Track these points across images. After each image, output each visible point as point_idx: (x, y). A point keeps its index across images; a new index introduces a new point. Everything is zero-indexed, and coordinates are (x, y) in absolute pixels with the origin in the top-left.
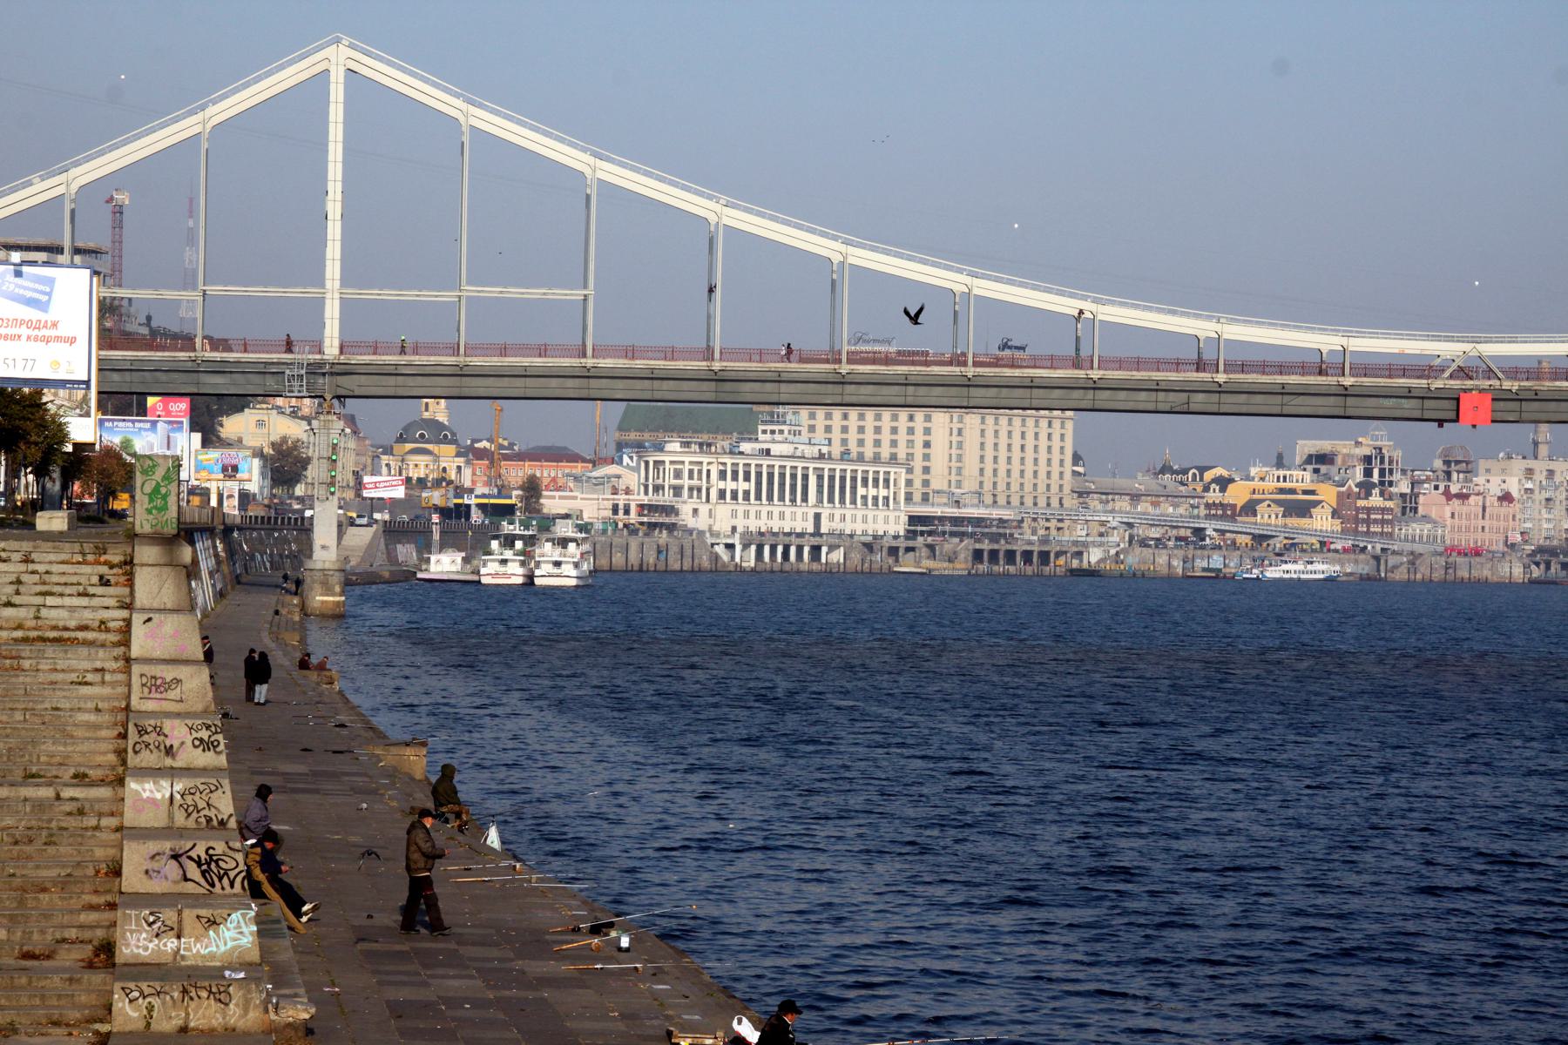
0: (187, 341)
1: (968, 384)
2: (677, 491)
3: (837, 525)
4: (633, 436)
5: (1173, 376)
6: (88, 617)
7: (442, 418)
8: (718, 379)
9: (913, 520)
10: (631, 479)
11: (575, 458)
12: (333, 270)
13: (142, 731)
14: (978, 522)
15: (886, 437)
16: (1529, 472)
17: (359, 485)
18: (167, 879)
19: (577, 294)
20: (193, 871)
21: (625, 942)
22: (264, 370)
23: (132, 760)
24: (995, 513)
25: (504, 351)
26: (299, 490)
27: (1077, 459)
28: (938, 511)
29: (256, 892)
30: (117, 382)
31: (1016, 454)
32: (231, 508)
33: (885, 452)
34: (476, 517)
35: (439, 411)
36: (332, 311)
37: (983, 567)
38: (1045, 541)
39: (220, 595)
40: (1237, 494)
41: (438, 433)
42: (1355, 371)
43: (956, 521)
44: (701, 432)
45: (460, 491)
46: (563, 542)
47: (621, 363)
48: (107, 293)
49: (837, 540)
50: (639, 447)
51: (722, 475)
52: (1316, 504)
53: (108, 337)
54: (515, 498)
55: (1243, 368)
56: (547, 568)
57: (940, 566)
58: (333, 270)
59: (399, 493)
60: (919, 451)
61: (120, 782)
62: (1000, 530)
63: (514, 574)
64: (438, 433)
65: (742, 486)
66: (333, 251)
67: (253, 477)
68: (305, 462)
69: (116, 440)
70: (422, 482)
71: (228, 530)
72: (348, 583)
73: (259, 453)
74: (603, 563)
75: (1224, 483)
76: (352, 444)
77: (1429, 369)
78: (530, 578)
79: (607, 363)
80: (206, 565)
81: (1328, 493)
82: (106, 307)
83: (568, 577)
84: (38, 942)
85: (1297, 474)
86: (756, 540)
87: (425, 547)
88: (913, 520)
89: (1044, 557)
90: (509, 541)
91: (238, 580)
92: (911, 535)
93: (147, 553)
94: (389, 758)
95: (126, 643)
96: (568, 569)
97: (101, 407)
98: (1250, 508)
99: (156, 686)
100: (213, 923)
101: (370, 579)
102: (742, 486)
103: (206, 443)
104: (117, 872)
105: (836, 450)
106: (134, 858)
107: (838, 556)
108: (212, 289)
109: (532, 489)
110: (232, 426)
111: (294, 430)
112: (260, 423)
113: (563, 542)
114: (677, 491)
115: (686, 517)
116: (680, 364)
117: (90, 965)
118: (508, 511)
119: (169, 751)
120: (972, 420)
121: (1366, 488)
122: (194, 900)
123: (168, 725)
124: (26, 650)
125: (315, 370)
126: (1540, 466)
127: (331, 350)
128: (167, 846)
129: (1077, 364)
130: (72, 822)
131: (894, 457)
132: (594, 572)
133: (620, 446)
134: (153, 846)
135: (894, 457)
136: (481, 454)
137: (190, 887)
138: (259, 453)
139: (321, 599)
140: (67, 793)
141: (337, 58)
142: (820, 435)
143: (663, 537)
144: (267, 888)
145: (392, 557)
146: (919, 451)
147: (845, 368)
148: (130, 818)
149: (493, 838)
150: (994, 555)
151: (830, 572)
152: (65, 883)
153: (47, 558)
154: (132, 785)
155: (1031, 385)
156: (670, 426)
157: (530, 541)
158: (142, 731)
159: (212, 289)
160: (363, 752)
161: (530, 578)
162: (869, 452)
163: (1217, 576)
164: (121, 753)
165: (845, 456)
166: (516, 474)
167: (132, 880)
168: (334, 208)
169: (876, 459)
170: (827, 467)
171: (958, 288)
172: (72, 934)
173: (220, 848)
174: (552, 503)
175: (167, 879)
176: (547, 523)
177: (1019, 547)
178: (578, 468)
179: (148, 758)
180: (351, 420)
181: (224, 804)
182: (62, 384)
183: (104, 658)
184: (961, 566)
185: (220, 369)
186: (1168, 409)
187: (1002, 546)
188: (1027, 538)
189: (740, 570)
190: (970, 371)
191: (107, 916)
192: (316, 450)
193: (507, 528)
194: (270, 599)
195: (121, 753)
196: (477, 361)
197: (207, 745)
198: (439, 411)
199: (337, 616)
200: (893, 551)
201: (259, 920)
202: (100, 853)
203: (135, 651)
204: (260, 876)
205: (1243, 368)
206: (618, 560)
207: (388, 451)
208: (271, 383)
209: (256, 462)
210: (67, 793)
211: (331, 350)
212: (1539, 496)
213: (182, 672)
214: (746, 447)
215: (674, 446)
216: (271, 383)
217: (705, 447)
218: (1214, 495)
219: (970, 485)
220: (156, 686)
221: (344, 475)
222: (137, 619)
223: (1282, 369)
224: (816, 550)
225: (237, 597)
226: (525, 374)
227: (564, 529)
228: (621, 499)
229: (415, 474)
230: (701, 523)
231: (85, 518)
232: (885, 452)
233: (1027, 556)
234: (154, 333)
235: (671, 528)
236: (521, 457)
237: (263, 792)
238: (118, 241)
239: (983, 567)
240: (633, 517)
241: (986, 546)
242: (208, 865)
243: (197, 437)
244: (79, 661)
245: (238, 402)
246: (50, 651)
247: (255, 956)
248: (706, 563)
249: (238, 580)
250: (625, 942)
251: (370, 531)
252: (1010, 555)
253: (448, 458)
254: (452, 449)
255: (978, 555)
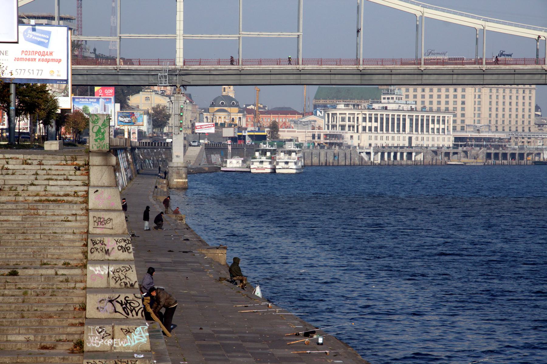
0: (113, 60)
1: (483, 73)
2: (343, 127)
3: (420, 143)
4: (322, 102)
6: (69, 190)
7: (232, 95)
8: (362, 73)
9: (457, 139)
10: (321, 122)
11: (294, 113)
12: (180, 26)
13: (94, 243)
14: (489, 139)
15: (443, 100)
17: (193, 126)
18: (107, 312)
19: (295, 35)
20: (119, 308)
21: (321, 340)
22: (149, 73)
23: (90, 256)
24: (497, 135)
25: (260, 62)
26: (166, 130)
27: (537, 108)
28: (469, 135)
29: (148, 317)
30: (81, 80)
32: (134, 138)
33: (443, 107)
34: (248, 141)
35: (230, 91)
37: (491, 162)
38: (522, 148)
39: (130, 179)
41: (230, 102)
43: (478, 139)
45: (240, 129)
46: (289, 153)
47: (316, 67)
48: (75, 38)
49: (421, 149)
50: (325, 107)
53: (76, 59)
54: (266, 132)
56: (282, 165)
57: (470, 161)
58: (180, 26)
59: (212, 130)
61: (85, 266)
62: (500, 143)
63: (267, 168)
64: (230, 102)
65: (374, 124)
66: (180, 17)
67: (145, 125)
68: (168, 117)
69: (80, 107)
70: (223, 125)
71: (133, 149)
72: (189, 173)
73: (147, 113)
74: (308, 162)
76: (190, 108)
78: (274, 169)
79: (309, 67)
80: (123, 165)
82: (75, 46)
83: (292, 169)
84: (48, 342)
86: (381, 150)
87: (224, 156)
88: (457, 139)
89: (521, 156)
90: (264, 152)
91: (138, 172)
92: (456, 146)
93: (95, 160)
94: (209, 254)
95: (86, 202)
96: (292, 165)
97: (73, 92)
99: (101, 222)
100: (128, 332)
101: (199, 171)
102: (374, 124)
103: (122, 108)
104: (84, 309)
105: (419, 106)
106: (92, 302)
107: (420, 157)
108: (124, 36)
109: (274, 127)
110: (134, 100)
111: (163, 101)
113: (289, 153)
114: (343, 127)
115: (347, 140)
117: (72, 352)
118: (263, 138)
119: (107, 252)
120: (485, 90)
122: (119, 321)
123: (106, 240)
124: (40, 206)
125: (172, 73)
127: (179, 63)
128: (107, 296)
129: (537, 62)
130: (63, 285)
132: (304, 166)
133: (315, 107)
134: (100, 296)
136: (250, 112)
137: (117, 315)
138: (147, 113)
139: (177, 180)
140: (61, 272)
142: (411, 100)
144: (153, 316)
145: (209, 161)
146: (459, 106)
147: (423, 67)
148: (89, 284)
149: (258, 292)
150: (496, 155)
151: (416, 164)
152: (61, 314)
153: (49, 163)
154: (90, 268)
155: (515, 73)
156: (339, 97)
157: (274, 152)
158: (94, 243)
159: (124, 36)
160: (197, 252)
161: (274, 169)
162: (435, 107)
163: (465, 165)
164: (85, 253)
165: (423, 109)
166: (267, 120)
167: (91, 312)
169: (439, 110)
172: (64, 337)
173: (131, 297)
174: (284, 134)
175: (107, 312)
176: (282, 144)
177: (509, 151)
178: (296, 117)
179: (98, 256)
180: (189, 97)
181: (133, 277)
182: (55, 81)
183: (77, 209)
184: (481, 161)
185: (128, 73)
187: (501, 151)
188: (513, 147)
189: (373, 164)
190: (484, 67)
191: (79, 329)
192: (173, 110)
193: (263, 146)
194: (153, 181)
195: (85, 253)
196: (247, 67)
197: (124, 249)
198: (230, 91)
199: (184, 189)
200: (447, 154)
201: (150, 331)
202: (76, 300)
203: (91, 206)
204: (150, 310)
206: (315, 160)
207: (207, 111)
208: (152, 80)
209: (145, 117)
210: (61, 272)
211: (179, 63)
213: (113, 215)
214: (375, 106)
216: (152, 80)
217: (356, 106)
219: (484, 122)
220: (101, 222)
221: (186, 123)
222: (92, 191)
224: (410, 154)
225: (138, 180)
226: (270, 73)
227: (290, 146)
228: (316, 132)
229: (219, 122)
230: (355, 142)
231: (66, 144)
232: (443, 107)
233: (513, 155)
234: (97, 57)
235: (340, 145)
236: (269, 112)
237: (151, 271)
238: (80, 14)
239: (491, 162)
240: (322, 140)
241: (493, 151)
242: (126, 305)
243: (118, 106)
244: (65, 210)
245: (137, 89)
246: (52, 206)
247: (148, 347)
248: (357, 162)
249: (138, 172)
250: (321, 340)
251: (198, 149)
252: (505, 156)
253: (235, 114)
255: (489, 156)
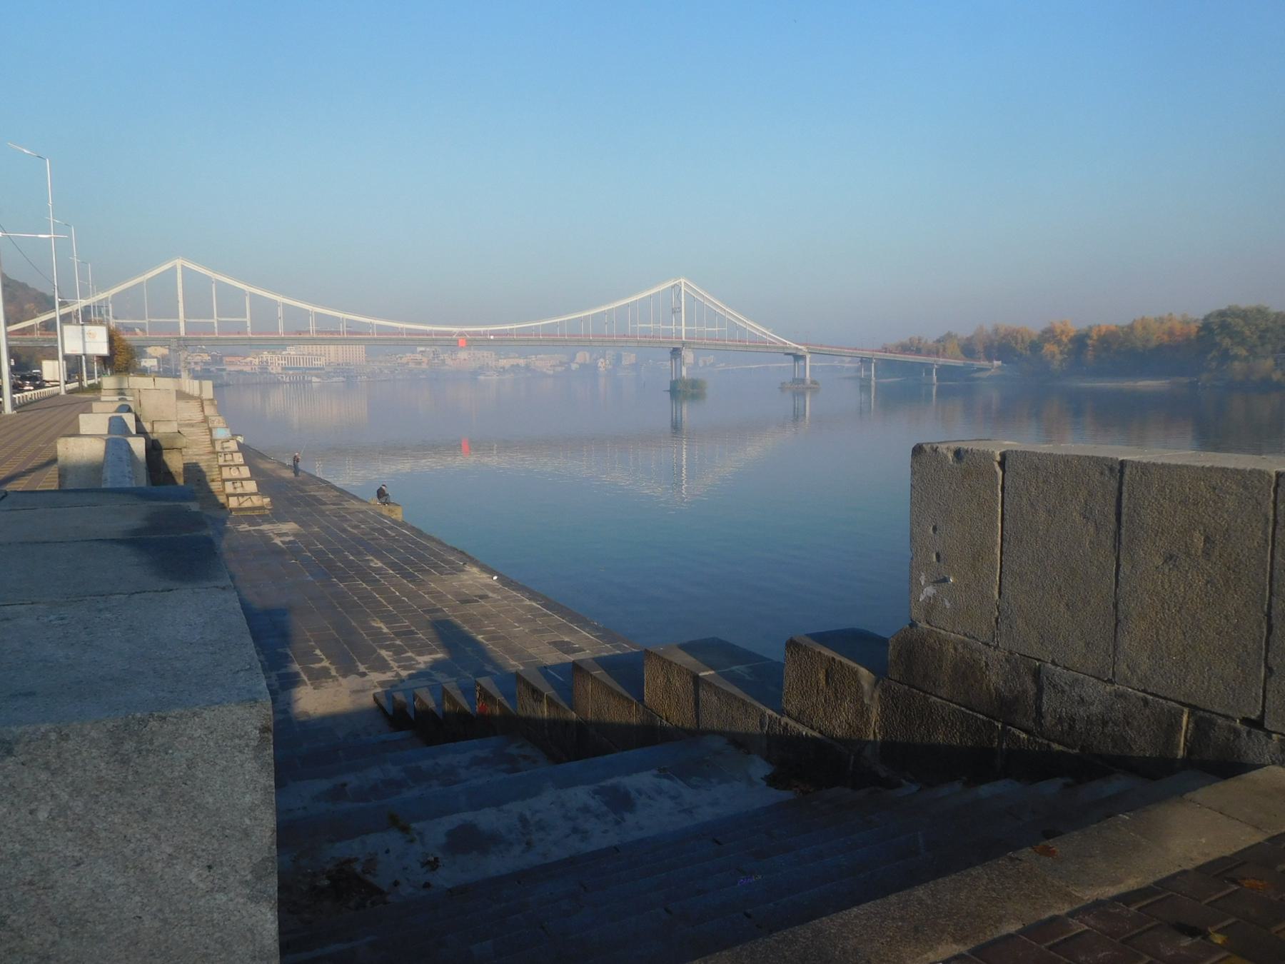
5: (394, 337)
12: (181, 314)
16: (470, 354)
25: (260, 334)
31: (351, 352)
36: (182, 325)
40: (404, 360)
42: (436, 335)
44: (995, 472)
51: (279, 360)
52: (423, 362)
55: (410, 334)
58: (181, 314)
60: (327, 353)
75: (401, 358)
77: (450, 334)
81: (425, 360)
85: (417, 355)
98: (408, 363)
112: (156, 350)
116: (263, 336)
121: (434, 358)
126: (472, 352)
127: (182, 333)
131: (321, 354)
135: (321, 354)
141: (179, 262)
143: (265, 375)
168: (180, 299)
169: (317, 355)
170: (305, 357)
171: (341, 317)
186: (1004, 550)
205: (410, 334)
212: (472, 359)
214: (284, 353)
215: (266, 353)
217: (274, 353)
218: (399, 361)
223: (419, 334)
254: (206, 355)
